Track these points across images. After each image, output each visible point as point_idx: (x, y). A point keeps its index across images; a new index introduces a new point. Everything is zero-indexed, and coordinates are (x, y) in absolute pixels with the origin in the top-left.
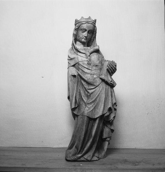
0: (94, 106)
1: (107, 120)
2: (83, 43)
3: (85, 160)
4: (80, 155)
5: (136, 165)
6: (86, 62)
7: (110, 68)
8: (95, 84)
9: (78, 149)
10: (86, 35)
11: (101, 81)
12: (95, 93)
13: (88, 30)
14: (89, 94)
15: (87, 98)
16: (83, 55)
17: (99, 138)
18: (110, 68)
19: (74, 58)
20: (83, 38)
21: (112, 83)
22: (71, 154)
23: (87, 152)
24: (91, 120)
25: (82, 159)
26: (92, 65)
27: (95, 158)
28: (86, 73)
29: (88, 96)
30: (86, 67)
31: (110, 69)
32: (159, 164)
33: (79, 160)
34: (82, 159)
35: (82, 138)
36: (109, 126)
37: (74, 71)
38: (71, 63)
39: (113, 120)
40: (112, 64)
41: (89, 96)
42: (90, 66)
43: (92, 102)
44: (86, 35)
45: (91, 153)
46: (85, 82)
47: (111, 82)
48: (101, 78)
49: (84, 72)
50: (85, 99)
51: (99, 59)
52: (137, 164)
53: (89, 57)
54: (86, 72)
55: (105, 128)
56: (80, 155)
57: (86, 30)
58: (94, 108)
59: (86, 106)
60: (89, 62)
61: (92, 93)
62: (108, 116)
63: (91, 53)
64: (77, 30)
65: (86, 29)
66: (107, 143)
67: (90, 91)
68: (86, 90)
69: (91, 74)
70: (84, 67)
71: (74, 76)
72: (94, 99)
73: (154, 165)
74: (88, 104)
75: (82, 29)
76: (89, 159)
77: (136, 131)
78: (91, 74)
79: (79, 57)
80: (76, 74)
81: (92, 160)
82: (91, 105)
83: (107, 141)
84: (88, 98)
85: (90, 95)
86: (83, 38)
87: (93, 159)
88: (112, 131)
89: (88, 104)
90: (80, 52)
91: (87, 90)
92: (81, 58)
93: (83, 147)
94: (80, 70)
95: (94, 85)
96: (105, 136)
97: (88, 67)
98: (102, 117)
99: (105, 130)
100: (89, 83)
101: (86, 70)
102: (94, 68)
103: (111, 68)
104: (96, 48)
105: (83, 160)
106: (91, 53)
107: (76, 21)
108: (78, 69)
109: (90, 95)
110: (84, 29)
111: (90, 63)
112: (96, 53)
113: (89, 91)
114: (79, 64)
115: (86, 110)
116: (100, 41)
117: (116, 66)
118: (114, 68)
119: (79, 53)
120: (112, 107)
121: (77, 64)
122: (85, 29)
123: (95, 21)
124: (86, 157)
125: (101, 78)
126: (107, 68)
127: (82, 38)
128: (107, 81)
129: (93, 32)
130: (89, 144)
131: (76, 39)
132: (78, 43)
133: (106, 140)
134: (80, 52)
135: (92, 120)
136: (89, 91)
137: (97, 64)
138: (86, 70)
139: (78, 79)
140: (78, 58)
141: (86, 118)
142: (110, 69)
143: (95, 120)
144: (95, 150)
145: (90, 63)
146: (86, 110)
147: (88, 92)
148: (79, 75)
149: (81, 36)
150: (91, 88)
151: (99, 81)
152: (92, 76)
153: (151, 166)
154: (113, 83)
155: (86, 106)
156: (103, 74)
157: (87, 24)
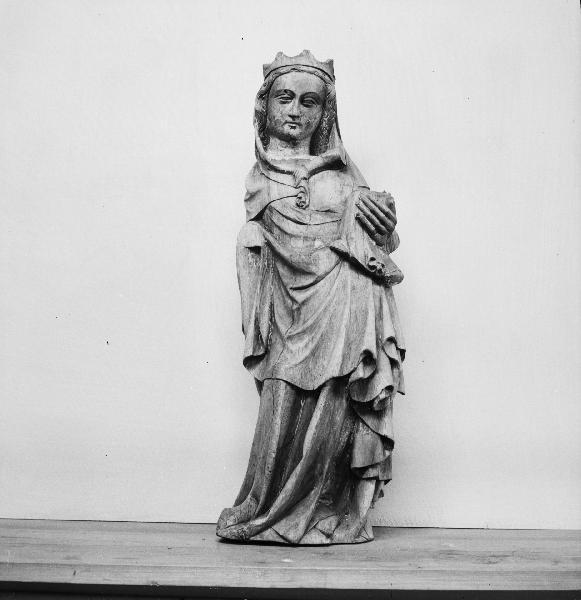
0: (311, 346)
1: (358, 399)
4: (260, 521)
5: (490, 563)
6: (293, 201)
7: (369, 213)
8: (313, 269)
9: (258, 501)
10: (299, 116)
11: (334, 257)
12: (314, 303)
13: (298, 94)
14: (295, 307)
15: (288, 320)
16: (287, 179)
18: (369, 213)
19: (259, 191)
20: (286, 122)
21: (374, 267)
22: (232, 517)
23: (287, 511)
24: (302, 397)
25: (268, 535)
26: (311, 207)
27: (316, 538)
28: (291, 236)
29: (293, 311)
30: (292, 215)
31: (368, 217)
33: (258, 538)
34: (268, 535)
35: (271, 460)
36: (370, 421)
37: (256, 236)
39: (385, 399)
40: (374, 199)
41: (294, 314)
42: (304, 212)
43: (304, 332)
44: (299, 116)
45: (301, 519)
46: (286, 268)
47: (372, 264)
48: (333, 249)
49: (286, 233)
50: (283, 328)
51: (341, 192)
52: (493, 560)
53: (303, 183)
54: (289, 232)
55: (357, 430)
56: (260, 521)
57: (292, 95)
58: (313, 353)
59: (284, 346)
60: (300, 198)
61: (303, 303)
62: (365, 384)
63: (314, 172)
64: (265, 95)
65: (293, 89)
66: (370, 487)
67: (300, 296)
68: (288, 294)
69: (306, 238)
71: (256, 250)
72: (310, 322)
73: (556, 562)
74: (290, 338)
75: (280, 91)
76: (292, 536)
78: (306, 238)
79: (274, 186)
80: (259, 244)
81: (302, 543)
82: (301, 344)
83: (369, 479)
85: (299, 309)
86: (286, 122)
87: (308, 540)
88: (388, 443)
89: (290, 338)
90: (277, 170)
91: (290, 292)
92: (279, 190)
93: (272, 495)
94: (276, 231)
95: (310, 274)
96: (359, 460)
97: (299, 215)
98: (339, 384)
99: (358, 437)
101: (290, 227)
102: (319, 218)
103: (373, 212)
104: (332, 153)
105: (271, 538)
106: (314, 172)
107: (265, 68)
109: (299, 309)
110: (286, 91)
111: (304, 202)
112: (331, 173)
113: (294, 294)
115: (290, 362)
116: (353, 136)
117: (391, 206)
118: (382, 215)
119: (273, 175)
120: (374, 350)
122: (292, 92)
123: (330, 63)
124: (281, 528)
125: (333, 249)
126: (358, 211)
128: (354, 258)
129: (323, 100)
130: (290, 484)
131: (266, 130)
132: (274, 141)
133: (365, 476)
134: (277, 170)
135: (307, 397)
136: (294, 294)
137: (332, 207)
138: (290, 227)
139: (274, 263)
141: (283, 391)
142: (368, 217)
143: (315, 394)
144: (318, 509)
145: (304, 202)
146: (290, 362)
147: (293, 300)
148: (268, 244)
149: (278, 116)
150: (300, 285)
151: (325, 261)
152: (309, 243)
153: (548, 566)
154: (379, 267)
155: (284, 346)
157: (294, 73)
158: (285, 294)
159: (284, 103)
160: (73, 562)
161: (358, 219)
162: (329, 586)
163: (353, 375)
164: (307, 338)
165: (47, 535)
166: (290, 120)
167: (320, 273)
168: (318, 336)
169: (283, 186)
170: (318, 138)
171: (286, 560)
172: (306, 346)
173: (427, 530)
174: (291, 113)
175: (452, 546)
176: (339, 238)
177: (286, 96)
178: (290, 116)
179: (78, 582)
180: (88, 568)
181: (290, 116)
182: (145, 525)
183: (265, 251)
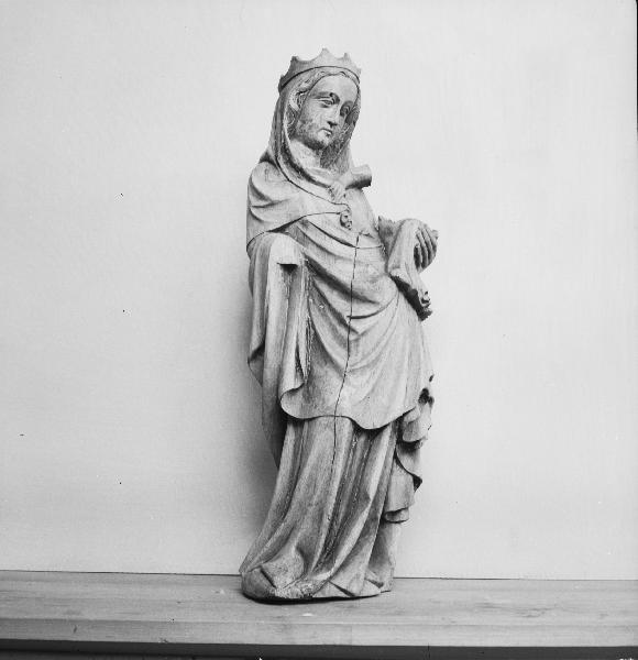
0: (373, 382)
2: (315, 146)
3: (342, 595)
8: (377, 298)
10: (311, 123)
13: (342, 101)
16: (323, 192)
17: (313, 560)
25: (331, 591)
32: (625, 613)
33: (319, 595)
38: (269, 220)
43: (368, 366)
44: (311, 123)
52: (534, 613)
54: (337, 254)
57: (337, 100)
61: (363, 334)
67: (358, 326)
68: (342, 321)
70: (331, 236)
73: (603, 615)
75: (324, 93)
77: (457, 544)
80: (294, 261)
84: (349, 350)
85: (357, 340)
89: (352, 371)
90: (310, 179)
91: (347, 321)
93: (331, 550)
100: (349, 294)
108: (304, 239)
109: (357, 340)
110: (331, 95)
114: (305, 224)
121: (297, 224)
124: (343, 581)
127: (320, 127)
136: (353, 324)
140: (301, 200)
142: (423, 249)
143: (374, 434)
147: (350, 329)
149: (316, 120)
156: (402, 265)
157: (341, 77)
158: (335, 322)
159: (326, 107)
160: (74, 617)
161: (416, 250)
162: (355, 643)
163: (405, 419)
164: (368, 373)
165: (45, 588)
166: (328, 127)
167: (384, 303)
168: (379, 372)
169: (320, 201)
170: (331, 152)
171: (307, 615)
172: (368, 382)
173: (403, 582)
174: (330, 119)
175: (489, 599)
176: (399, 267)
177: (330, 99)
178: (329, 123)
179: (80, 639)
180: (150, 625)
181: (329, 123)
182: (184, 577)
183: (304, 273)
